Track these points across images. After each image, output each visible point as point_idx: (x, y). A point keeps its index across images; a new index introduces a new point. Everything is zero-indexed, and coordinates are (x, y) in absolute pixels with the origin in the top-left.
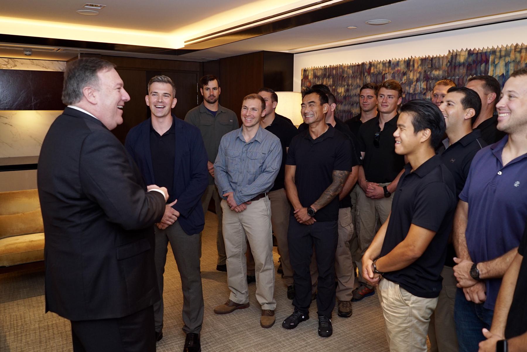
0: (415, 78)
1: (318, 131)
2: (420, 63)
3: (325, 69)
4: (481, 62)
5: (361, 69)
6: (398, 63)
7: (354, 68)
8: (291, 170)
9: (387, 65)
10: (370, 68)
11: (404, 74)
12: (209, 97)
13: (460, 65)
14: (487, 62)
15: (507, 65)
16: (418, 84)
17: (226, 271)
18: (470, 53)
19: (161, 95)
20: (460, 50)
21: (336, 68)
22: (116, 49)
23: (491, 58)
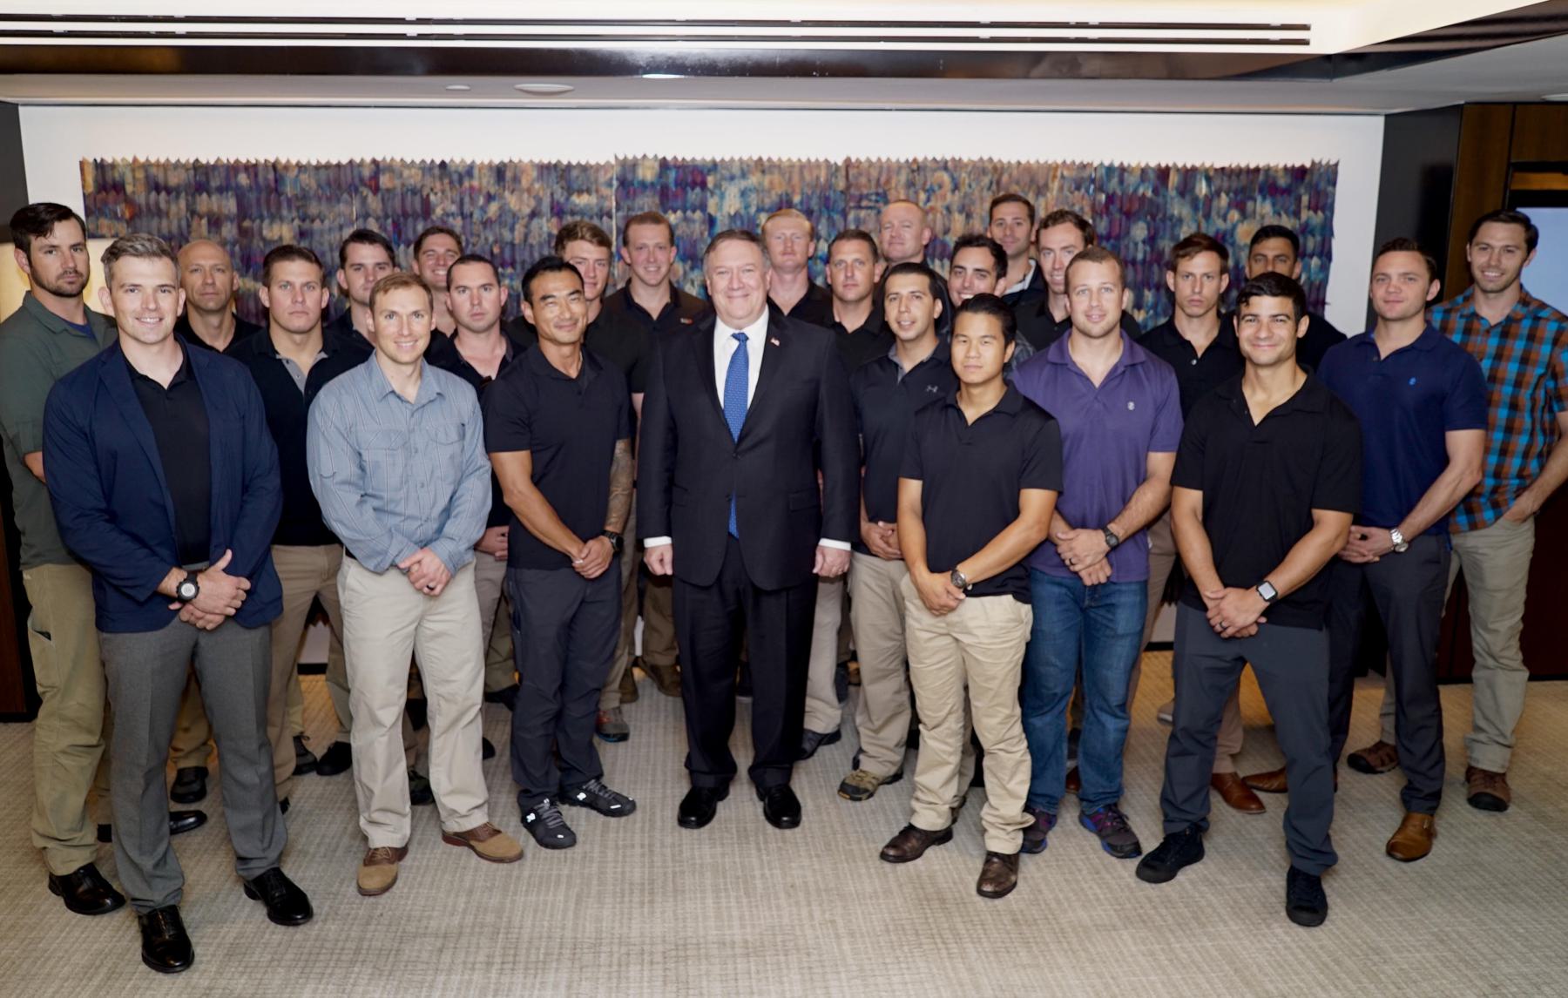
0: (527, 211)
1: (1397, 338)
2: (535, 174)
3: (197, 166)
4: (694, 185)
5: (343, 181)
6: (469, 171)
7: (323, 174)
8: (515, 465)
9: (437, 171)
10: (375, 177)
11: (490, 198)
12: (59, 277)
13: (643, 185)
14: (703, 185)
15: (743, 194)
16: (535, 222)
17: (434, 801)
18: (664, 164)
19: (150, 291)
20: (639, 156)
21: (251, 169)
22: (1085, 71)
23: (710, 180)
